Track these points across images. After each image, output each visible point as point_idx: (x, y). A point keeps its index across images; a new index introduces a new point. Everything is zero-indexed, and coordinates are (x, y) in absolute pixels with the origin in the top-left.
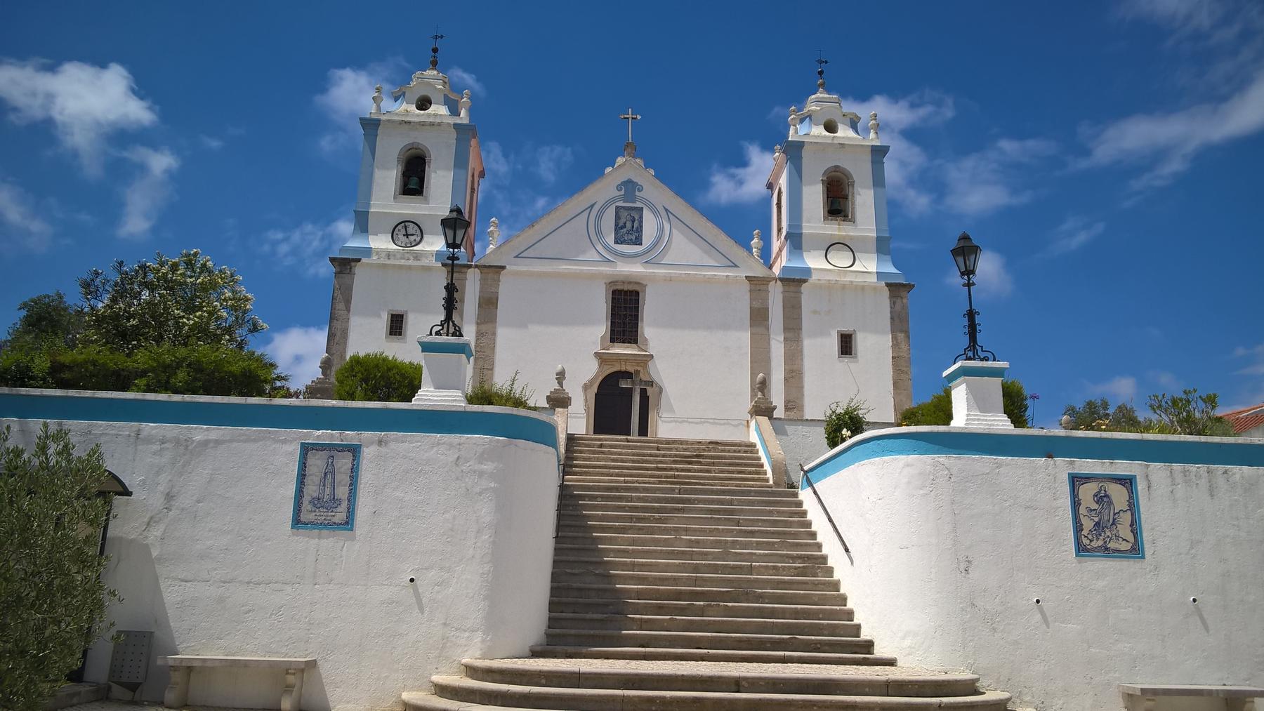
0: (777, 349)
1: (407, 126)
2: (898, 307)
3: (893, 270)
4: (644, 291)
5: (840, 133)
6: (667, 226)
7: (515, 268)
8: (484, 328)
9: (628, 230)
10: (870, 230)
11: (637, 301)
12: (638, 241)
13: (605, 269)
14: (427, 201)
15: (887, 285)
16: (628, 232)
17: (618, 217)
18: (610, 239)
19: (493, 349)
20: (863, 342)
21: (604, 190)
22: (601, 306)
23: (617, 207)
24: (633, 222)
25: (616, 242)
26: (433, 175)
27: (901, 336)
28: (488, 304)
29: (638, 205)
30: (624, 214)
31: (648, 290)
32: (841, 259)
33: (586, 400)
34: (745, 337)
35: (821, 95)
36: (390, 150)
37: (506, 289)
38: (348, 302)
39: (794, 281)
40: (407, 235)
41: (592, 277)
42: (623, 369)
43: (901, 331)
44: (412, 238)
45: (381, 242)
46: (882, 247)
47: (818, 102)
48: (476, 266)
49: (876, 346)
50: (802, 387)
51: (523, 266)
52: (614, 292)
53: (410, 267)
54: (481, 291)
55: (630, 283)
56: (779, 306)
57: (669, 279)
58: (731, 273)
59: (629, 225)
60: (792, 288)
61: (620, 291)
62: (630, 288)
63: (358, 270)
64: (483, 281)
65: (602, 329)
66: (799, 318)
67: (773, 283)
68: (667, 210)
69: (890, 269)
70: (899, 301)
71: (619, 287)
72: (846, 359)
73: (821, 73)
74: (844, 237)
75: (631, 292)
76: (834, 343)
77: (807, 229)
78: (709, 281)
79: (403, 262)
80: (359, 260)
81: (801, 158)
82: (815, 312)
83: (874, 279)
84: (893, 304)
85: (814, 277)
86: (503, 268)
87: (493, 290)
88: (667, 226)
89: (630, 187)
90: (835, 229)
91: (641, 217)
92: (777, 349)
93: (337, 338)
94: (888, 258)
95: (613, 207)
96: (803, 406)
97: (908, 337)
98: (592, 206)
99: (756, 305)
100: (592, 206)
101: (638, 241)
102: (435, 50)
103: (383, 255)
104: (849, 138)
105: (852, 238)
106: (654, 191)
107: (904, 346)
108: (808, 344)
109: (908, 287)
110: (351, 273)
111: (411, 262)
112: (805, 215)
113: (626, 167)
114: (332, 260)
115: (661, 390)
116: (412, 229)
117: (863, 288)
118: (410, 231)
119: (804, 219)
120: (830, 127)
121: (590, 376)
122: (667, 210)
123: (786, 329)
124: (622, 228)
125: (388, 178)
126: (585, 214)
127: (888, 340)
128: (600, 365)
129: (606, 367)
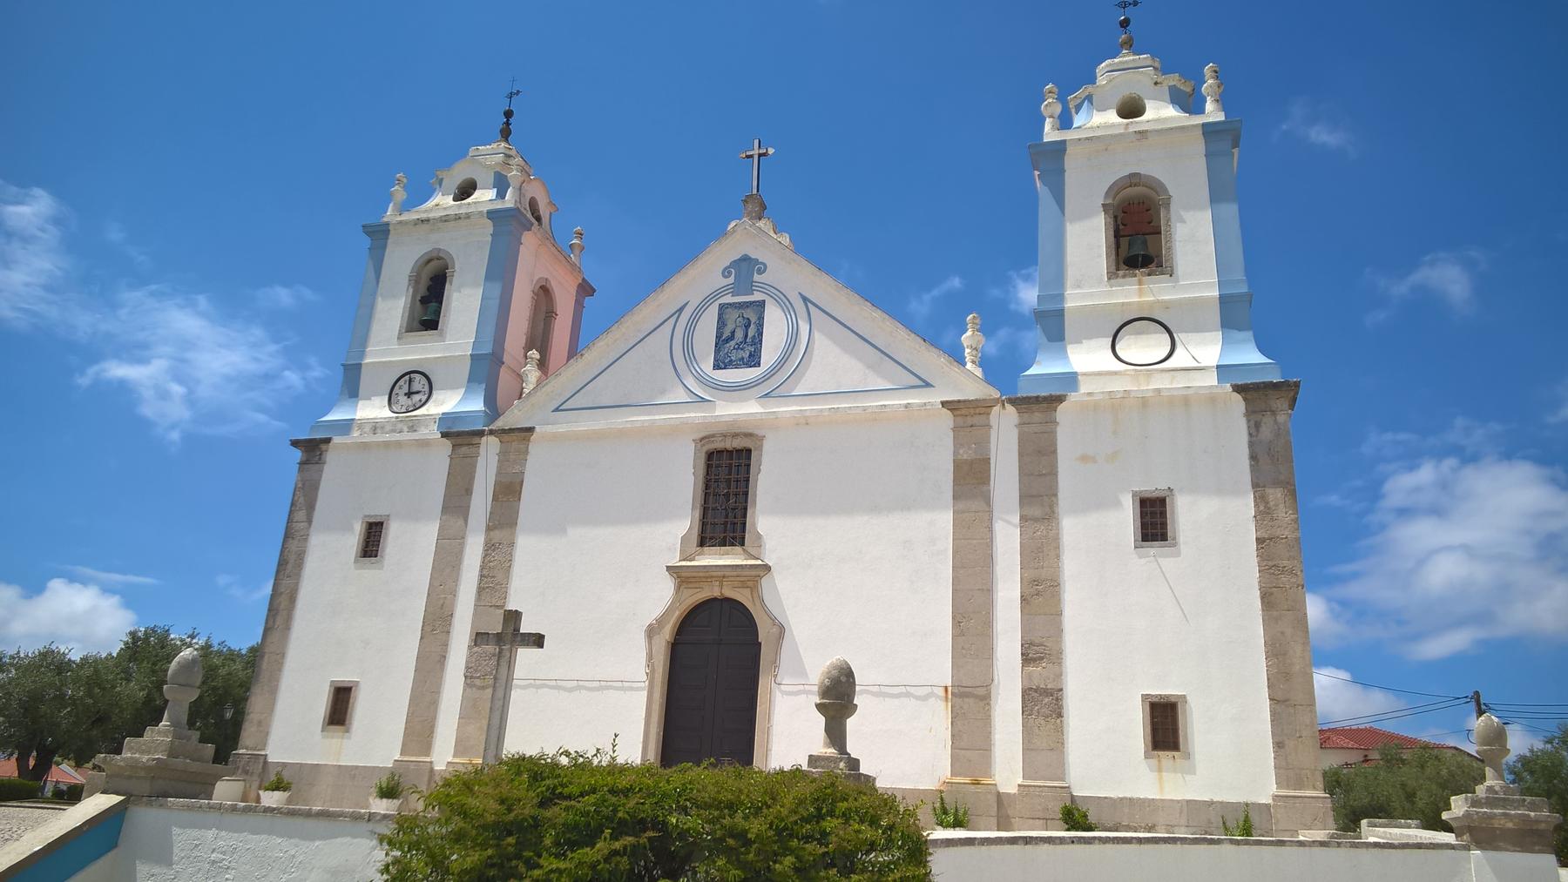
0: (1007, 538)
1: (426, 226)
2: (1266, 432)
3: (1256, 357)
4: (760, 448)
5: (1149, 115)
6: (804, 328)
7: (550, 429)
8: (497, 535)
9: (738, 342)
10: (1208, 286)
12: (754, 360)
13: (696, 415)
14: (442, 337)
15: (1238, 389)
16: (738, 348)
17: (721, 323)
18: (707, 365)
19: (508, 571)
20: (1186, 514)
21: (704, 278)
22: (683, 481)
23: (722, 307)
24: (747, 326)
25: (717, 367)
26: (455, 295)
27: (1276, 495)
28: (508, 491)
29: (757, 297)
30: (733, 317)
31: (767, 446)
32: (1143, 348)
33: (650, 657)
34: (944, 520)
35: (1126, 58)
36: (401, 262)
38: (311, 507)
39: (1042, 405)
40: (409, 394)
41: (673, 431)
42: (717, 594)
43: (1277, 483)
44: (416, 398)
45: (373, 409)
46: (1233, 314)
47: (1118, 72)
48: (491, 432)
49: (1221, 523)
50: (1060, 614)
52: (710, 456)
53: (399, 444)
54: (499, 473)
55: (735, 435)
56: (1007, 457)
57: (803, 422)
58: (915, 399)
59: (739, 335)
60: (1037, 416)
61: (720, 452)
62: (738, 443)
63: (332, 457)
64: (503, 456)
65: (684, 524)
66: (1053, 473)
67: (996, 409)
68: (805, 299)
69: (1251, 355)
70: (1267, 421)
71: (719, 445)
72: (1154, 549)
73: (1125, 24)
74: (1151, 305)
75: (739, 451)
76: (1126, 518)
77: (1074, 299)
78: (877, 418)
79: (397, 437)
80: (328, 441)
81: (1062, 171)
82: (1084, 458)
83: (1211, 380)
84: (1254, 428)
85: (1084, 388)
86: (531, 430)
87: (517, 469)
88: (804, 328)
89: (745, 269)
90: (1134, 293)
91: (761, 318)
92: (1007, 538)
93: (290, 566)
94: (1249, 334)
95: (712, 314)
96: (1061, 652)
97: (1293, 494)
98: (681, 310)
99: (966, 455)
100: (681, 310)
101: (754, 360)
102: (509, 114)
103: (367, 429)
104: (1166, 120)
105: (1167, 306)
106: (786, 270)
107: (1284, 514)
108: (1071, 528)
109: (1288, 390)
111: (407, 436)
112: (1071, 273)
113: (749, 237)
114: (295, 443)
115: (782, 630)
116: (419, 383)
117: (1185, 401)
118: (416, 386)
119: (1069, 282)
120: (1130, 109)
121: (657, 611)
122: (805, 299)
123: (1026, 498)
125: (393, 308)
127: (1244, 507)
128: (678, 589)
129: (686, 593)
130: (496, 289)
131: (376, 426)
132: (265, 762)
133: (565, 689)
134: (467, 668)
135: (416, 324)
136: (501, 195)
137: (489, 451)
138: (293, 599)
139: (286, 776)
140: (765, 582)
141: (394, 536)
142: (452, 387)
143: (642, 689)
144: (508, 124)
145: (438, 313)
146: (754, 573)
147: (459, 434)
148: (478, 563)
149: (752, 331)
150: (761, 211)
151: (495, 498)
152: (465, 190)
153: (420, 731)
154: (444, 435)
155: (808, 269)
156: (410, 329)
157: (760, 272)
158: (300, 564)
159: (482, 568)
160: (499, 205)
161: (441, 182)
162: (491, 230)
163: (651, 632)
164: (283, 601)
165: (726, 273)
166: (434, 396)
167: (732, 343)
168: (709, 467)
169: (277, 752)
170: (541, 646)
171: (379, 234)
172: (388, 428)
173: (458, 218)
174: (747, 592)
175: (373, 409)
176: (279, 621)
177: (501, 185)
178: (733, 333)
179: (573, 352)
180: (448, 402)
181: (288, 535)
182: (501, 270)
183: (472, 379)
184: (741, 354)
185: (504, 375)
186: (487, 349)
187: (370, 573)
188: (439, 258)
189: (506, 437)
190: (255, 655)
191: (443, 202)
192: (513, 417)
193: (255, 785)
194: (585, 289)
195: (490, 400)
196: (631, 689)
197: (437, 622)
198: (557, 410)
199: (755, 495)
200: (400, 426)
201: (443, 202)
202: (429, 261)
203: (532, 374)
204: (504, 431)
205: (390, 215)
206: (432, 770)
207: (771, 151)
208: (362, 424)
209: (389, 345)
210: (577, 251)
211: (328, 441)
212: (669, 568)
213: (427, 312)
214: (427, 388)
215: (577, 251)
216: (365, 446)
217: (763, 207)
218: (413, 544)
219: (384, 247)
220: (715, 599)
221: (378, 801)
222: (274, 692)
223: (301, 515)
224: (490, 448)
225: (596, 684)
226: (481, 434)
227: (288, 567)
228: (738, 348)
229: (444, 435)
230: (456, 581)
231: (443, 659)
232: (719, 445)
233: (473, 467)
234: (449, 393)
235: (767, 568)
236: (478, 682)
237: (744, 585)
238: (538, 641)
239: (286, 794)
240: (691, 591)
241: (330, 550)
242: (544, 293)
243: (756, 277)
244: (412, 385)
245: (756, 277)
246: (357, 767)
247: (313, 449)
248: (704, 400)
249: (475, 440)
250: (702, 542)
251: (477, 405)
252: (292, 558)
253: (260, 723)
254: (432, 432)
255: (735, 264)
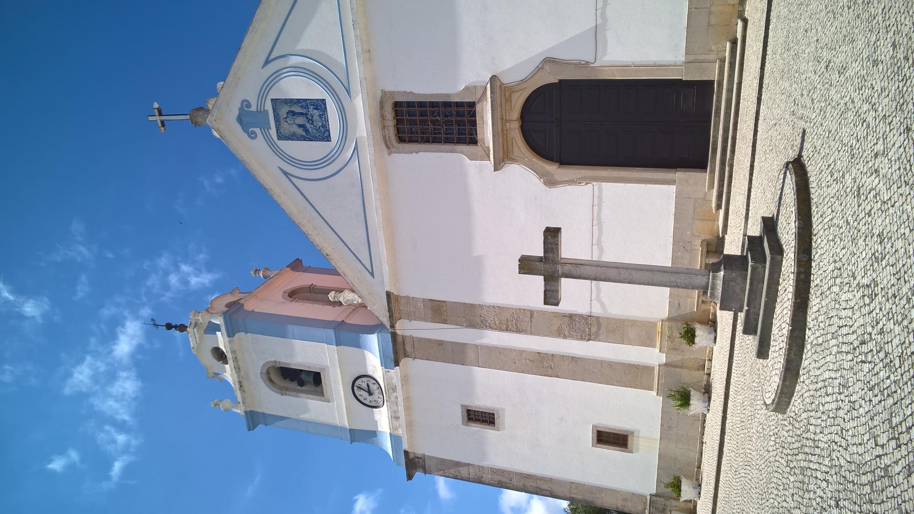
0: (493, 338)
1: (245, 384)
4: (392, 94)
6: (294, 60)
7: (386, 279)
9: (306, 120)
11: (410, 104)
12: (320, 105)
13: (368, 154)
17: (292, 137)
19: (502, 309)
21: (258, 154)
23: (281, 137)
24: (294, 114)
25: (328, 139)
28: (439, 311)
29: (269, 107)
31: (390, 87)
33: (571, 182)
36: (273, 401)
37: (416, 288)
38: (458, 464)
45: (382, 419)
48: (392, 326)
51: (384, 268)
52: (401, 140)
53: (407, 399)
55: (383, 117)
61: (398, 131)
62: (390, 114)
63: (422, 448)
64: (411, 317)
68: (267, 62)
75: (397, 114)
80: (406, 453)
86: (388, 295)
87: (421, 305)
89: (248, 119)
93: (503, 479)
95: (288, 146)
98: (286, 174)
100: (286, 174)
101: (320, 105)
102: (169, 326)
103: (396, 423)
106: (244, 83)
110: (423, 458)
111: (400, 393)
113: (223, 121)
114: (410, 477)
115: (549, 61)
118: (364, 386)
122: (267, 62)
124: (307, 131)
125: (310, 408)
126: (294, 179)
128: (513, 160)
130: (291, 328)
131: (394, 417)
132: (656, 495)
133: (600, 234)
134: (582, 339)
135: (318, 389)
136: (217, 328)
137: (413, 328)
138: (529, 477)
139: (670, 480)
140: (507, 80)
141: (482, 402)
142: (364, 359)
143: (600, 190)
144: (176, 327)
145: (308, 373)
146: (498, 91)
147: (396, 352)
148: (497, 333)
149: (297, 109)
150: (204, 110)
151: (444, 322)
152: (220, 355)
153: (633, 376)
154: (397, 363)
155: (240, 61)
156: (321, 394)
157: (249, 106)
158: (501, 472)
159: (502, 330)
160: (223, 328)
161: (217, 374)
162: (243, 334)
163: (551, 182)
164: (531, 484)
165: (252, 136)
166: (370, 373)
167: (308, 126)
168: (411, 141)
169: (649, 487)
170: (557, 231)
171: (254, 419)
172: (395, 408)
173: (235, 359)
174: (515, 96)
175: (382, 419)
176: (545, 487)
177: (212, 329)
178: (300, 126)
179: (334, 272)
180: (374, 363)
181: (479, 481)
182: (277, 326)
183: (357, 344)
184: (316, 118)
185: (355, 320)
186: (331, 333)
187: (507, 419)
188: (268, 373)
189: (396, 315)
190: (572, 500)
191: (229, 373)
192: (380, 310)
193: (674, 503)
194: (296, 265)
195: (370, 330)
196: (600, 197)
197: (544, 364)
198: (372, 274)
199: (431, 95)
200: (393, 399)
201: (229, 373)
202: (271, 380)
203: (347, 297)
204: (391, 316)
205: (240, 411)
206: (666, 365)
207: (156, 105)
208: (393, 428)
209: (335, 408)
210: (269, 273)
211: (406, 453)
212: (496, 169)
213: (308, 380)
214: (364, 379)
215: (269, 273)
216: (410, 425)
217: (201, 109)
218: (489, 386)
219: (264, 414)
220: (522, 128)
221: (692, 407)
222: (600, 490)
223: (464, 472)
224: (405, 328)
225: (596, 228)
226: (394, 335)
227: (505, 480)
228: (311, 121)
229: (397, 363)
230: (511, 350)
231: (574, 359)
232: (391, 132)
233: (420, 339)
234: (368, 362)
235: (493, 79)
236: (594, 330)
237: (509, 100)
238: (552, 235)
239: (684, 480)
240: (516, 149)
241: (498, 449)
242: (293, 294)
243: (253, 109)
244: (362, 389)
245: (253, 109)
246: (662, 425)
247: (414, 464)
248: (356, 148)
249: (400, 339)
250: (474, 141)
251: (373, 340)
252: (497, 478)
253: (625, 500)
254: (395, 372)
255: (245, 129)
